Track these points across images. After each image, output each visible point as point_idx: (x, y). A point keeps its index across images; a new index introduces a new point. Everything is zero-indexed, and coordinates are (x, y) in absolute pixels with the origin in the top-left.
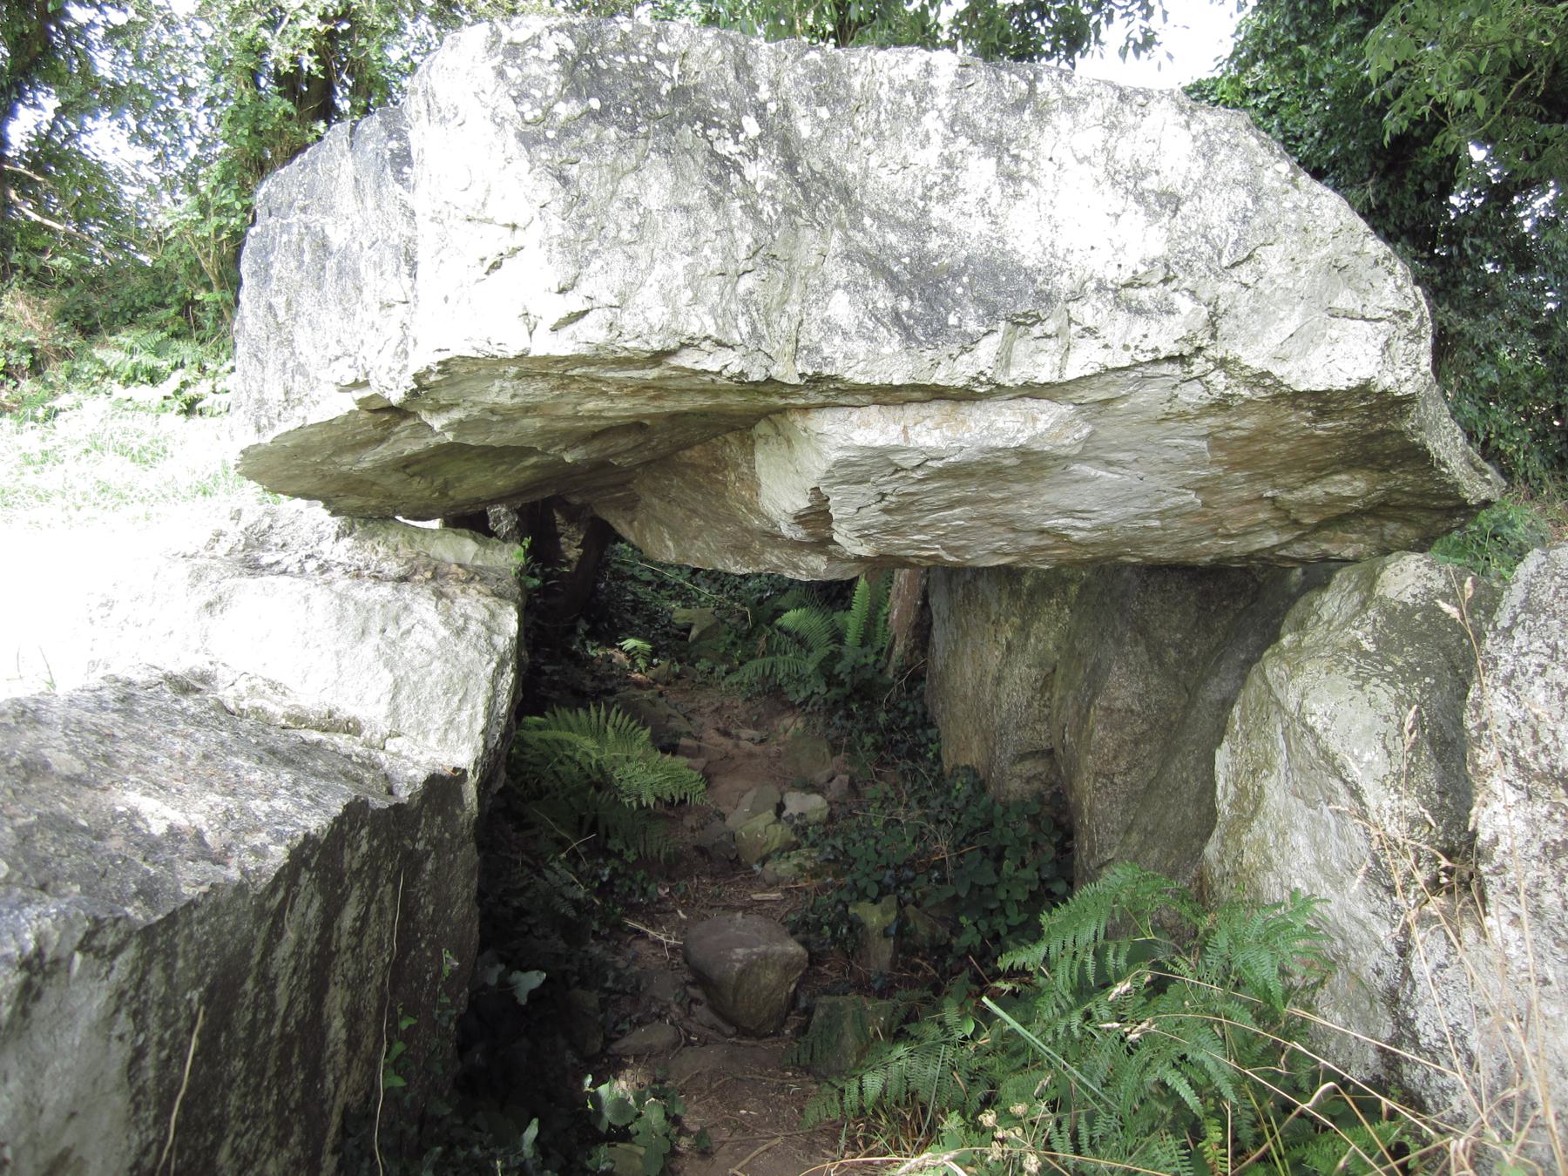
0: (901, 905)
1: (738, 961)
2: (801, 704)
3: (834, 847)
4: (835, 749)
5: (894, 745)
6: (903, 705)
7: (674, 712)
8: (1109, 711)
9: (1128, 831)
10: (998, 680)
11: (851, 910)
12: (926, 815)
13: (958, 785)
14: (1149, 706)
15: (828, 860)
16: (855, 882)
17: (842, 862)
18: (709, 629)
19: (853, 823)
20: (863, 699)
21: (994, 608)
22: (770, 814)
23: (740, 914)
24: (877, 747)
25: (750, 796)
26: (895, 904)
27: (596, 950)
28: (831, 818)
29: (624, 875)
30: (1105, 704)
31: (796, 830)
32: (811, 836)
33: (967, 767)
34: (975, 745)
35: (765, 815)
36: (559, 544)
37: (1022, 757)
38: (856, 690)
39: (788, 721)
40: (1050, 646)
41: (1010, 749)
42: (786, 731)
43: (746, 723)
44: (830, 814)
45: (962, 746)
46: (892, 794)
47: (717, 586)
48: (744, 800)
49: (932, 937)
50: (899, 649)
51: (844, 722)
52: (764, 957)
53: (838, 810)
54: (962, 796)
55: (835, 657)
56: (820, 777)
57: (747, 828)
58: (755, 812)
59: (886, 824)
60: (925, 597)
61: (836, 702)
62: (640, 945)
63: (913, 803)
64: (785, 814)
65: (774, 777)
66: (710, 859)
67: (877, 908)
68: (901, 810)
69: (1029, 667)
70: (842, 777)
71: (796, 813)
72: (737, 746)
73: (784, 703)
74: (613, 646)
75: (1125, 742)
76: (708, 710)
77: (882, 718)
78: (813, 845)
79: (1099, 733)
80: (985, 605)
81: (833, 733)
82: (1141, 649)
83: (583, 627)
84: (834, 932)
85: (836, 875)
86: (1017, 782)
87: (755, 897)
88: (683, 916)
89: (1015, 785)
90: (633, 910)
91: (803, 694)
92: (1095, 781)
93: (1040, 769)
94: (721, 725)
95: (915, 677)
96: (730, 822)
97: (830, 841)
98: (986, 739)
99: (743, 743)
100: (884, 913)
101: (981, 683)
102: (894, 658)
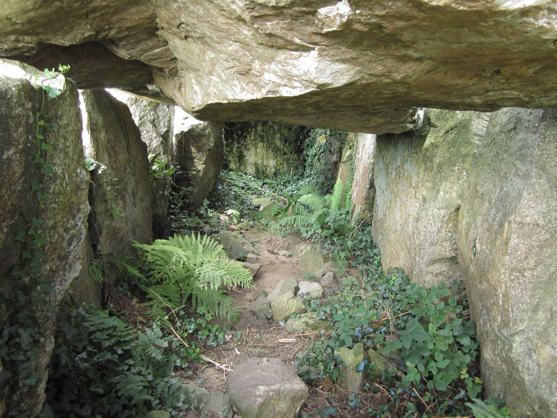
0: (366, 349)
1: (260, 396)
2: (309, 238)
3: (325, 312)
4: (326, 259)
5: (355, 257)
6: (360, 238)
7: (246, 242)
8: (521, 224)
9: (535, 310)
10: (417, 220)
11: (336, 353)
12: (377, 294)
13: (394, 278)
14: (550, 221)
15: (322, 319)
16: (338, 335)
17: (330, 320)
18: (268, 206)
19: (336, 298)
20: (339, 235)
21: (415, 179)
22: (290, 294)
23: (265, 359)
24: (347, 258)
25: (281, 283)
26: (362, 350)
27: (174, 380)
28: (324, 295)
29: (206, 328)
30: (518, 219)
31: (304, 302)
32: (313, 306)
33: (397, 268)
34: (402, 256)
35: (287, 294)
36: (193, 162)
37: (434, 262)
38: (336, 231)
39: (303, 247)
40: (454, 195)
41: (426, 258)
42: (302, 252)
43: (282, 248)
44: (323, 293)
45: (393, 256)
46: (356, 283)
47: (274, 190)
48: (278, 285)
49: (386, 371)
50: (357, 211)
51: (330, 246)
52: (278, 393)
53: (327, 291)
54: (396, 284)
55: (325, 215)
56: (318, 273)
57: (278, 301)
58: (283, 292)
59: (354, 299)
60: (372, 186)
61: (326, 237)
62: (211, 371)
63: (369, 288)
64: (299, 293)
65: (294, 273)
66: (258, 318)
67: (351, 351)
68: (362, 291)
69: (439, 209)
70: (330, 273)
71: (305, 293)
72: (277, 258)
73: (301, 238)
74: (222, 213)
75: (533, 247)
76: (264, 242)
77: (350, 243)
78: (314, 311)
79: (514, 241)
80: (409, 178)
81: (325, 252)
82: (543, 181)
83: (206, 202)
84: (325, 367)
85: (326, 328)
86: (430, 276)
87: (280, 340)
88: (238, 353)
89: (429, 278)
90: (207, 349)
91: (310, 233)
92: (511, 274)
93: (444, 269)
94: (270, 249)
95: (365, 225)
96: (269, 298)
97: (323, 308)
98: (409, 252)
99: (280, 257)
100: (356, 355)
101: (406, 222)
102: (354, 215)
